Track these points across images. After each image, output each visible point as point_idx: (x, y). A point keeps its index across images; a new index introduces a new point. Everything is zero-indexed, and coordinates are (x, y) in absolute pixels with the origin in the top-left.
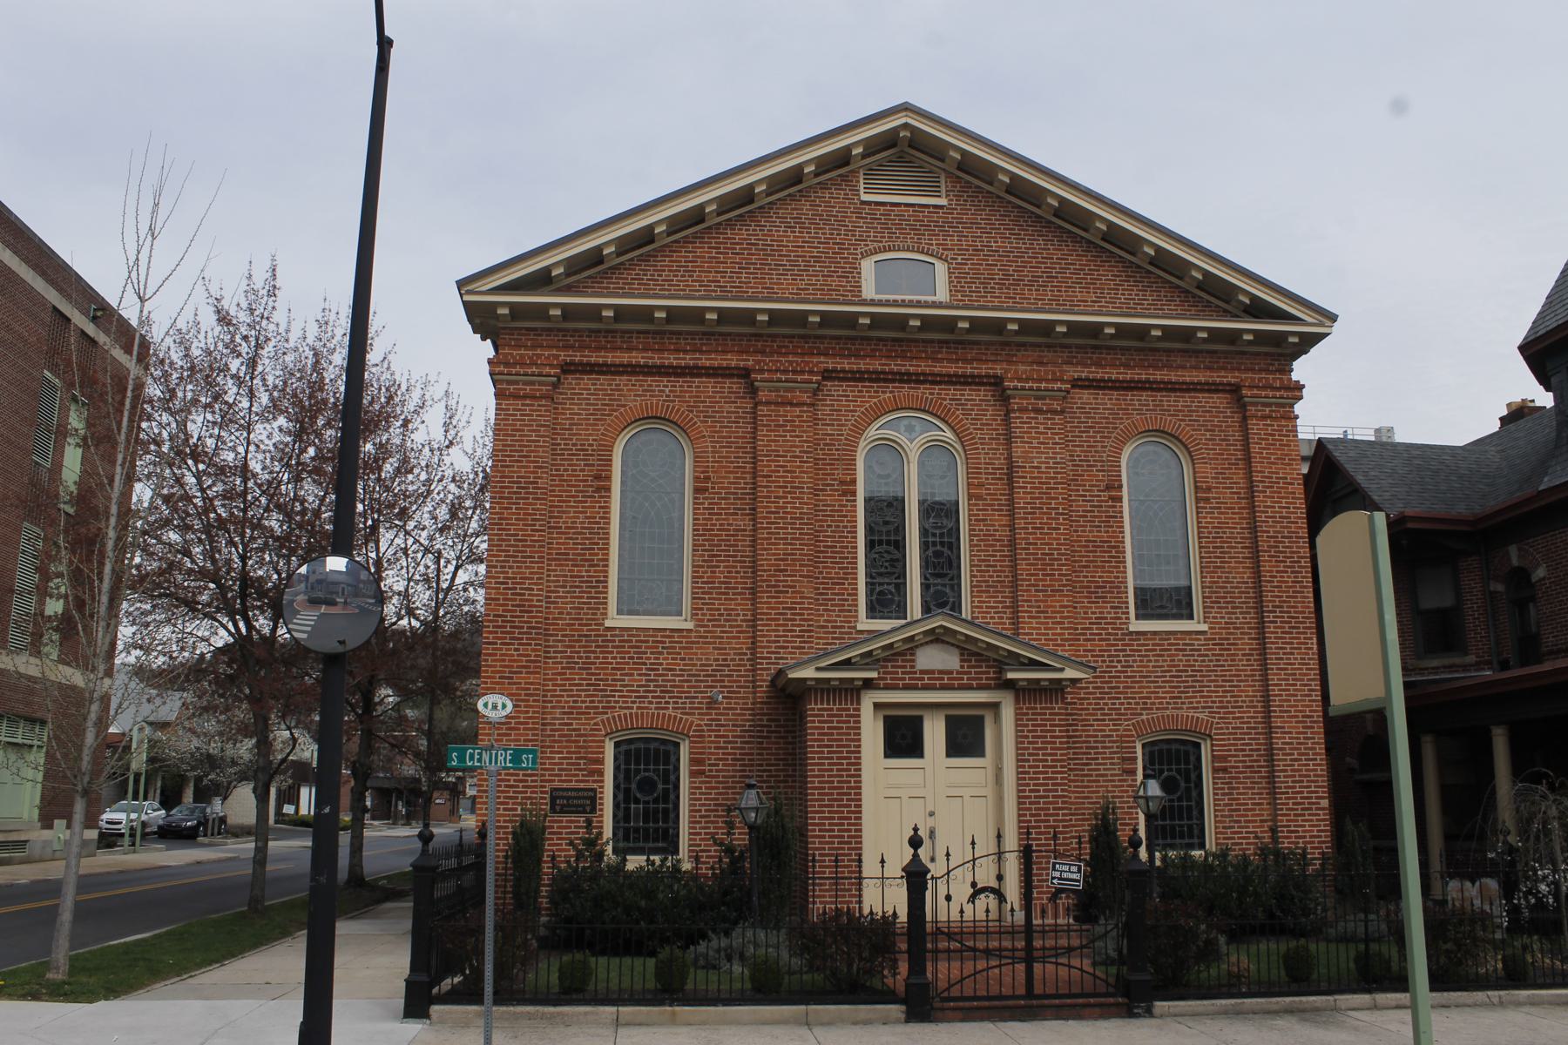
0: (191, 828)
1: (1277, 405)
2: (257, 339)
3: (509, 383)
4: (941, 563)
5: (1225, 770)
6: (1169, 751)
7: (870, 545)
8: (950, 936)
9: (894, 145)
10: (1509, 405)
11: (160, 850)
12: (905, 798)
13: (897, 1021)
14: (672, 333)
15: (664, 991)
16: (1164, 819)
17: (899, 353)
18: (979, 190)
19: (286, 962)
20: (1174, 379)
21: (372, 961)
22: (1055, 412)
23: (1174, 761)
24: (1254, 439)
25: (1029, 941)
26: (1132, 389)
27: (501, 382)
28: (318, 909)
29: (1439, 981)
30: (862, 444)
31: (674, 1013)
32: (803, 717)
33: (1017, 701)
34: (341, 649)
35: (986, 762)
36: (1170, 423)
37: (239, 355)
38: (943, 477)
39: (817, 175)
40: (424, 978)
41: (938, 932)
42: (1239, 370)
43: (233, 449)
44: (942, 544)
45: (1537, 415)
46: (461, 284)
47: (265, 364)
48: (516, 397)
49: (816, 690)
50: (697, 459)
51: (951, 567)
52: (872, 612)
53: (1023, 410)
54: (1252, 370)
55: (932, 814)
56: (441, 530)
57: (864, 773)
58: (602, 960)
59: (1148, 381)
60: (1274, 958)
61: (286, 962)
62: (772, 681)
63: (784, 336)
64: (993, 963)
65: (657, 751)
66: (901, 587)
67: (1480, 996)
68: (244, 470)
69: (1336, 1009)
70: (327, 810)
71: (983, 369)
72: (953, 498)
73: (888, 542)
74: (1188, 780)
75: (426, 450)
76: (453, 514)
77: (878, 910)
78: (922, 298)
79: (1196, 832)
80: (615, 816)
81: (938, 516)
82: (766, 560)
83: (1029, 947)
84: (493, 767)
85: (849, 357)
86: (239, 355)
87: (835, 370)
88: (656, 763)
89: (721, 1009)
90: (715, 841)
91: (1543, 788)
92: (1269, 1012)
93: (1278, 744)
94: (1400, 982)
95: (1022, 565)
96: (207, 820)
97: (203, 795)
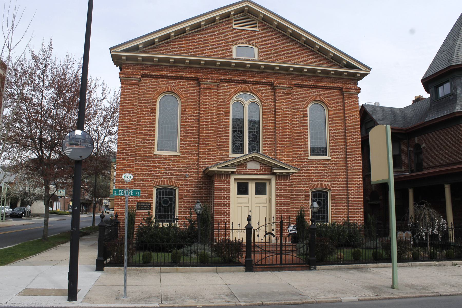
0: (20, 214)
1: (353, 94)
2: (45, 64)
3: (125, 80)
4: (254, 137)
5: (334, 200)
6: (319, 194)
7: (233, 132)
8: (258, 247)
9: (243, 12)
10: (415, 97)
11: (11, 221)
12: (243, 207)
13: (243, 271)
14: (175, 66)
15: (174, 262)
16: (319, 214)
17: (243, 74)
18: (268, 27)
19: (62, 253)
20: (323, 85)
21: (88, 254)
22: (289, 94)
23: (320, 196)
24: (346, 104)
25: (281, 248)
26: (311, 88)
27: (123, 79)
28: (74, 237)
29: (400, 260)
30: (231, 101)
31: (177, 269)
32: (213, 182)
33: (276, 178)
34: (80, 159)
35: (267, 196)
36: (322, 98)
37: (40, 69)
38: (255, 112)
39: (220, 20)
40: (102, 259)
41: (255, 246)
42: (342, 83)
43: (37, 98)
44: (254, 132)
45: (424, 100)
46: (111, 49)
47: (48, 72)
48: (127, 84)
49: (217, 174)
50: (182, 105)
51: (257, 139)
52: (233, 152)
53: (279, 93)
54: (346, 83)
55: (250, 211)
56: (100, 125)
57: (231, 199)
58: (156, 254)
59: (316, 86)
60: (351, 255)
61: (62, 253)
62: (203, 171)
63: (209, 68)
64: (271, 254)
65: (169, 192)
66: (242, 145)
67: (406, 264)
68: (41, 105)
69: (367, 268)
70: (76, 208)
71: (268, 80)
72: (258, 119)
73: (239, 131)
74: (324, 202)
75: (96, 101)
76: (104, 121)
77: (237, 239)
78: (251, 58)
79: (326, 217)
80: (156, 211)
81: (253, 124)
82: (202, 136)
83: (281, 250)
84: (127, 195)
85: (228, 75)
86: (40, 69)
87: (224, 79)
88: (169, 195)
89: (191, 268)
90: (186, 218)
91: (424, 206)
92: (348, 269)
93: (350, 192)
94: (389, 260)
95: (278, 139)
96: (25, 212)
97: (24, 204)
